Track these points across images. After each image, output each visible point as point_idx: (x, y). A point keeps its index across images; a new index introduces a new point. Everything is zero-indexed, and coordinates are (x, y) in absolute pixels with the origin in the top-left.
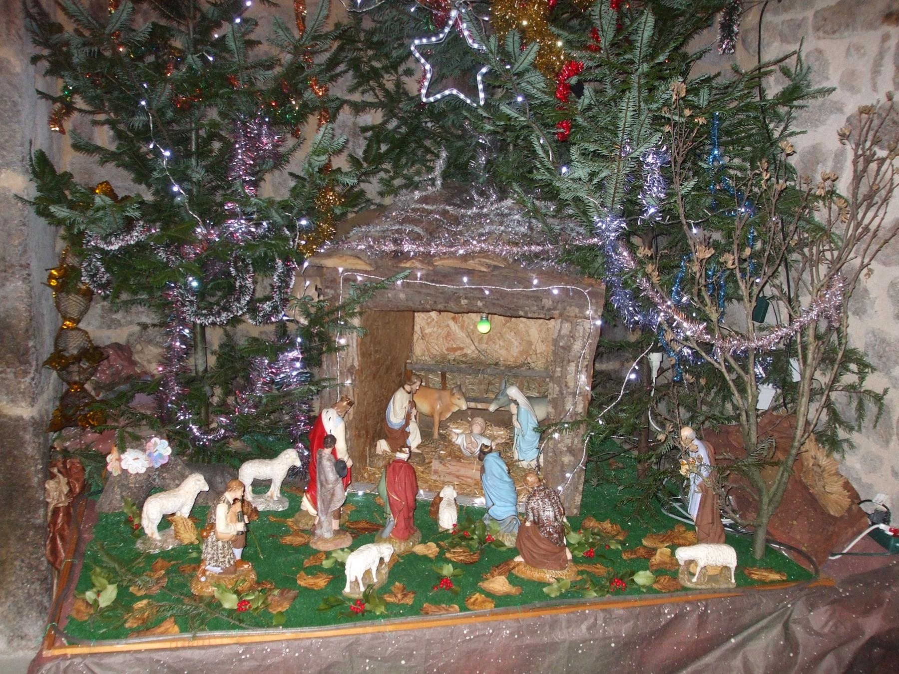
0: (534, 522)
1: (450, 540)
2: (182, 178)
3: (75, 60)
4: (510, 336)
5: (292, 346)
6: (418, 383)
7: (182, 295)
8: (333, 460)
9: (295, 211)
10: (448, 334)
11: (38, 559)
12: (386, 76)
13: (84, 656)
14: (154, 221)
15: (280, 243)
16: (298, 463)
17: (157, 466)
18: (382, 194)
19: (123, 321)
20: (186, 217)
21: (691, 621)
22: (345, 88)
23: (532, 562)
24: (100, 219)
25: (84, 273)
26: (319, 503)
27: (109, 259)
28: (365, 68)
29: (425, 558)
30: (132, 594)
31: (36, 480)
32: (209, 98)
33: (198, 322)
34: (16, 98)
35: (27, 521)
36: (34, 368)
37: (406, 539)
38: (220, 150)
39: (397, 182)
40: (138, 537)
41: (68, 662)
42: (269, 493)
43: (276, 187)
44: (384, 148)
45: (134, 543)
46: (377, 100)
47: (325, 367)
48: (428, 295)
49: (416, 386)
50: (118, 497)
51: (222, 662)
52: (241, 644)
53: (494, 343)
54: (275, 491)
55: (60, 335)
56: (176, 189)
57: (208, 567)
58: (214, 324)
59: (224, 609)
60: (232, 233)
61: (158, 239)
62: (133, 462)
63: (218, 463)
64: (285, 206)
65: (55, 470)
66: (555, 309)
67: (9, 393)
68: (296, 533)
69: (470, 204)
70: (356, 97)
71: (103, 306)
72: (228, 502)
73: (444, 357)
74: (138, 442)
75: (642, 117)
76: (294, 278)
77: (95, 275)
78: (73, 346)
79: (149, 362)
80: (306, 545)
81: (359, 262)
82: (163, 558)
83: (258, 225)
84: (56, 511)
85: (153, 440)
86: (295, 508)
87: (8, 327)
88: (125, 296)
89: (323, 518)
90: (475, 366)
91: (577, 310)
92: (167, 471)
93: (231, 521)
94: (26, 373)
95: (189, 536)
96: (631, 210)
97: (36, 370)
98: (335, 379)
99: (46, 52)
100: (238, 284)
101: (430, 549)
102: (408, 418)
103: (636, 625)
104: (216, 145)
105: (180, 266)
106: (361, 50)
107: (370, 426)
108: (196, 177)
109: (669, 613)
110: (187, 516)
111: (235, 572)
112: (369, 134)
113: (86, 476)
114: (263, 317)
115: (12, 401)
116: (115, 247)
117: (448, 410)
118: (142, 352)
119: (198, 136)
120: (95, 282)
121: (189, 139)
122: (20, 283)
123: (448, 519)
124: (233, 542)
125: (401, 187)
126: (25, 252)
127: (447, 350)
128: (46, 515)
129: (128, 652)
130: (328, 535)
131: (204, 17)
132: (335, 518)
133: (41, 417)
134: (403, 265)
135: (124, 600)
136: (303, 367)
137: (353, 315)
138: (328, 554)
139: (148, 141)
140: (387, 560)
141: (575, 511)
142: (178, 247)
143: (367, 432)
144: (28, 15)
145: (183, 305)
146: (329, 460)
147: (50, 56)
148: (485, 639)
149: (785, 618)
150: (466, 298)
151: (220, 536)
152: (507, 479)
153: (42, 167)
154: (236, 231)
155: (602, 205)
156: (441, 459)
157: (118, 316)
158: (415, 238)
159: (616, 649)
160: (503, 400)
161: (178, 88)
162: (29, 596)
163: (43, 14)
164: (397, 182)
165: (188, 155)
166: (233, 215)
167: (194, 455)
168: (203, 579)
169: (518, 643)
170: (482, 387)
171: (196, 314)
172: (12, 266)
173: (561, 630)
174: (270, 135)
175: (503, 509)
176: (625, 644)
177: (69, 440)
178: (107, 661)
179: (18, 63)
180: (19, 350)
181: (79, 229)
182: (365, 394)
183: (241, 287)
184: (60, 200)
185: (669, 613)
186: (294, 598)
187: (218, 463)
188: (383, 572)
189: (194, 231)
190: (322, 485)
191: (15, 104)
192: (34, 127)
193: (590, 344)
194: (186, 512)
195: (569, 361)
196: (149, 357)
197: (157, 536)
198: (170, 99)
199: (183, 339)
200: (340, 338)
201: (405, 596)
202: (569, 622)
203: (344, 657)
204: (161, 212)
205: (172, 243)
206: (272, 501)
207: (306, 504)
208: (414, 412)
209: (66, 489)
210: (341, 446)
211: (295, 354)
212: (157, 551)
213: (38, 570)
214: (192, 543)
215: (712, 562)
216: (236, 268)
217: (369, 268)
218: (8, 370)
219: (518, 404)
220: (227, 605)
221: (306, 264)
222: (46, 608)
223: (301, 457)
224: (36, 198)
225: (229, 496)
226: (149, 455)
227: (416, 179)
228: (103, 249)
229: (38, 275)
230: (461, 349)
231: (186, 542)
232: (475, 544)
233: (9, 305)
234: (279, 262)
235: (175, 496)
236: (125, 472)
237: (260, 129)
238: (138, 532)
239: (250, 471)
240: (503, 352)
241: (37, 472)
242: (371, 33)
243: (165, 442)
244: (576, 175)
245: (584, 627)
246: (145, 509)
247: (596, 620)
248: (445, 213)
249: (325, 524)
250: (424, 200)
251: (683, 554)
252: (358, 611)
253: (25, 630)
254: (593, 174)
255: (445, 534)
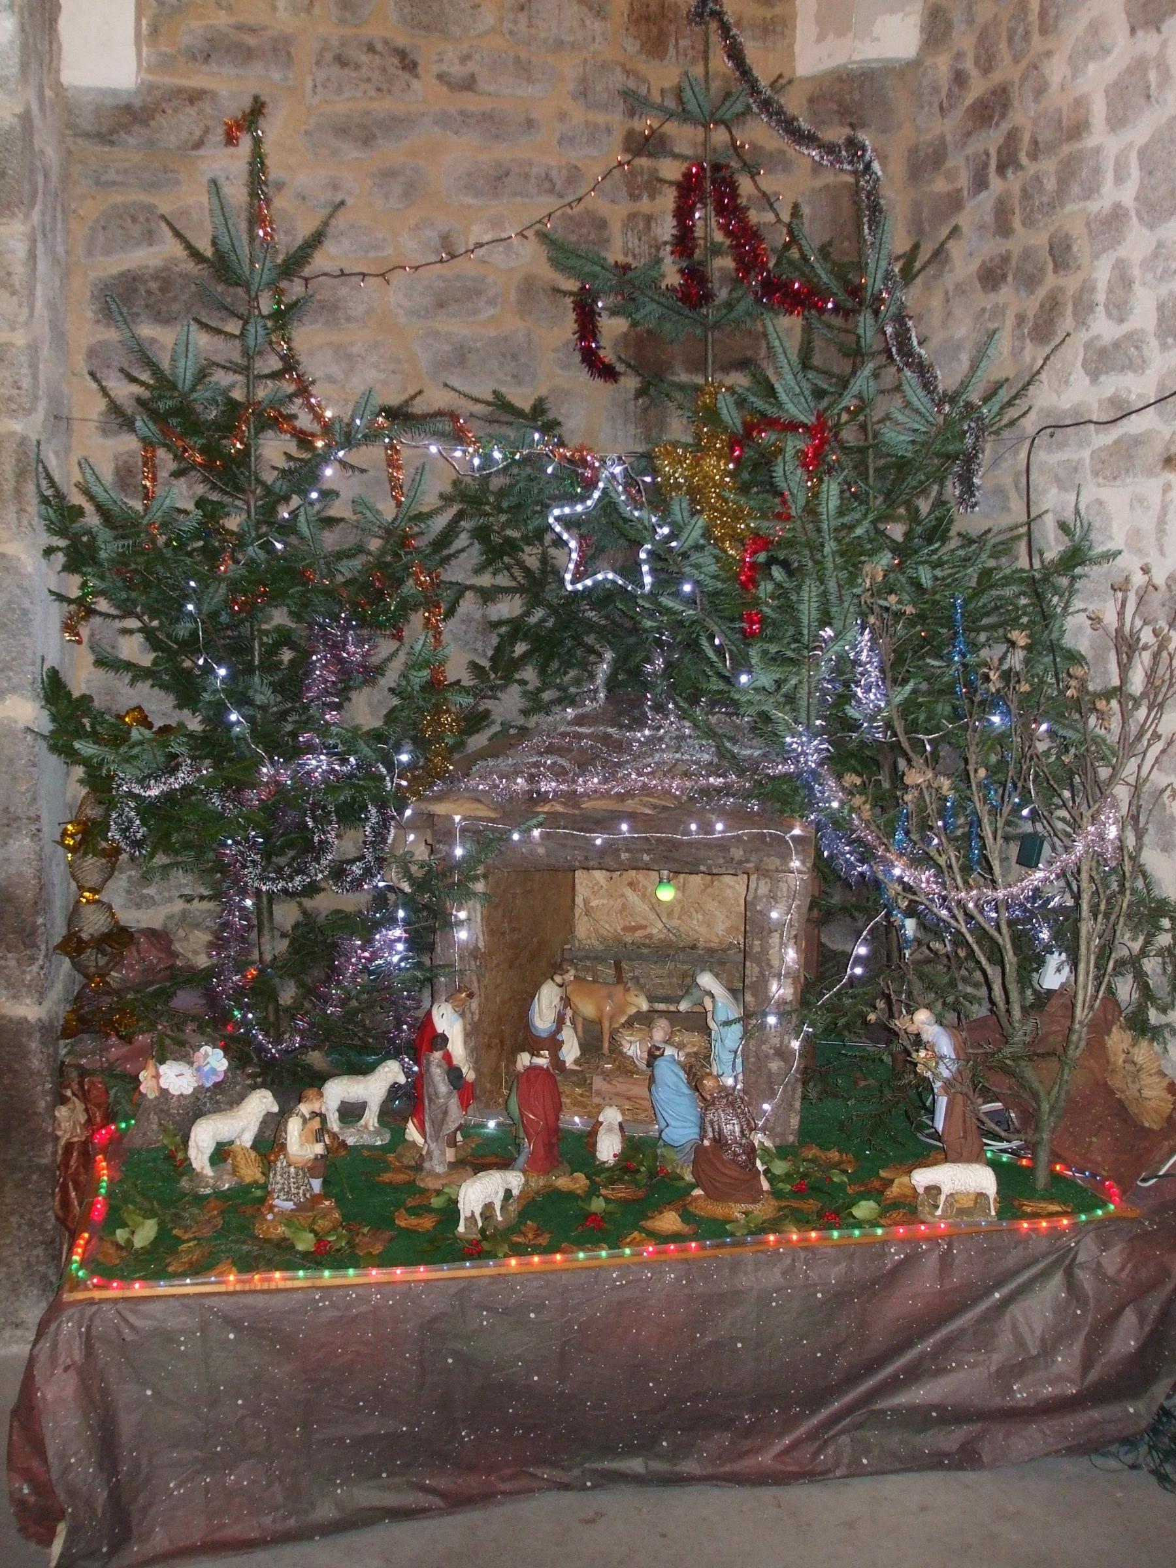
0: (714, 1139)
1: (607, 1174)
2: (242, 700)
3: (103, 555)
4: (712, 906)
5: (392, 921)
6: (572, 972)
7: (242, 853)
8: (446, 1067)
9: (392, 742)
10: (624, 907)
11: (43, 1213)
12: (527, 549)
13: (115, 1301)
14: (201, 758)
15: (371, 784)
16: (402, 1080)
17: (208, 1085)
18: (525, 713)
19: (157, 897)
20: (247, 752)
21: (931, 1263)
22: (469, 567)
23: (714, 1194)
24: (136, 757)
25: (113, 827)
26: (427, 1125)
27: (148, 809)
28: (496, 539)
29: (571, 1195)
30: (177, 1238)
31: (43, 1104)
32: (277, 598)
33: (264, 888)
34: (27, 604)
35: (30, 1161)
36: (43, 953)
37: (546, 1172)
38: (291, 661)
39: (547, 696)
40: (182, 1175)
41: (94, 1308)
42: (362, 1122)
43: (366, 709)
44: (520, 648)
45: (178, 1181)
46: (514, 584)
47: (439, 950)
48: (575, 848)
49: (570, 976)
50: (155, 1127)
51: (293, 1311)
52: (318, 1288)
53: (691, 917)
54: (371, 1118)
55: (74, 915)
56: (233, 717)
57: (276, 1202)
58: (285, 891)
59: (298, 1252)
60: (308, 773)
61: (210, 782)
62: (175, 1079)
63: (293, 1082)
64: (377, 736)
65: (69, 1093)
66: (748, 861)
67: (10, 985)
68: (399, 1170)
69: (640, 723)
70: (485, 580)
71: (130, 877)
72: (303, 1116)
73: (619, 940)
74: (182, 1051)
75: (846, 605)
76: (393, 831)
77: (128, 829)
78: (94, 923)
79: (196, 953)
80: (411, 1183)
81: (480, 806)
82: (217, 1198)
83: (344, 761)
84: (69, 1147)
85: (203, 1050)
86: (399, 1135)
87: (10, 899)
88: (161, 859)
89: (433, 1146)
90: (663, 951)
91: (778, 861)
92: (223, 1092)
93: (307, 1141)
94: (32, 959)
95: (251, 1172)
96: (840, 725)
97: (46, 956)
98: (452, 965)
99: (62, 543)
100: (316, 839)
101: (576, 1182)
102: (560, 1021)
103: (850, 1269)
104: (287, 655)
105: (239, 816)
106: (489, 515)
107: (504, 1031)
108: (260, 699)
109: (896, 1253)
110: (248, 1145)
111: (312, 1209)
112: (503, 630)
113: (111, 1100)
114: (352, 882)
115: (14, 997)
116: (154, 792)
117: (623, 1012)
118: (186, 938)
119: (262, 644)
120: (127, 838)
121: (251, 650)
122: (27, 841)
123: (608, 1148)
124: (311, 1169)
125: (552, 702)
126: (34, 800)
127: (624, 929)
128: (55, 1153)
129: (173, 1296)
130: (440, 1169)
131: (268, 490)
132: (449, 1146)
133: (51, 1021)
134: (539, 809)
135: (165, 1244)
136: (407, 950)
137: (476, 878)
138: (438, 1193)
139: (197, 652)
140: (516, 1192)
141: (791, 1138)
142: (238, 791)
143: (502, 1042)
144: (45, 500)
145: (244, 867)
146: (439, 1066)
147: (68, 547)
148: (643, 1285)
149: (1067, 1262)
150: (627, 851)
151: (292, 1159)
152: (686, 1091)
153: (54, 689)
154: (315, 770)
155: (796, 722)
156: (606, 1075)
157: (151, 891)
158: (559, 773)
159: (823, 1302)
160: (696, 994)
161: (234, 586)
162: (29, 1265)
163: (60, 496)
164: (547, 696)
165: (249, 670)
166: (310, 749)
167: (254, 1066)
168: (270, 1217)
169: (686, 1291)
170: (675, 980)
171: (263, 878)
172: (18, 818)
173: (746, 1273)
174: (359, 643)
175: (682, 1132)
176: (837, 1295)
177: (85, 1056)
178: (143, 1308)
179: (30, 561)
180: (24, 929)
181: (109, 770)
182: (497, 987)
183: (321, 842)
184: (80, 733)
185: (896, 1253)
186: (392, 1239)
187: (293, 1082)
188: (511, 1208)
189: (258, 771)
190: (430, 1100)
191: (25, 612)
192: (47, 640)
193: (798, 907)
194: (247, 1140)
195: (771, 931)
196: (195, 947)
197: (209, 1171)
198: (225, 601)
199: (244, 913)
200: (458, 910)
201: (537, 1235)
202: (756, 1264)
203: (453, 1307)
204: (213, 744)
205: (229, 786)
206: (369, 1132)
207: (412, 1133)
208: (569, 1013)
209: (83, 1118)
210: (457, 1048)
211: (398, 932)
212: (208, 1191)
213: (43, 1230)
214: (256, 1182)
215: (959, 1187)
216: (314, 818)
217: (493, 815)
218: (10, 955)
219: (713, 997)
220: (300, 1247)
221: (408, 813)
222: (51, 1283)
223: (408, 1073)
224: (52, 732)
225: (304, 1108)
226: (198, 1070)
227: (572, 690)
228: (139, 795)
229: (50, 831)
230: (644, 927)
231: (248, 1180)
232: (642, 1178)
233: (12, 870)
234: (373, 810)
235: (233, 1118)
236: (164, 1092)
237: (344, 635)
238: (185, 1167)
239: (338, 1091)
240: (703, 930)
241: (45, 1093)
242: (502, 493)
243: (220, 1053)
244: (758, 684)
245: (777, 1271)
246: (192, 1135)
247: (793, 1260)
248: (606, 738)
249: (436, 1154)
250: (579, 720)
251: (922, 1178)
252: (475, 1251)
253: (22, 1314)
254: (779, 683)
255: (601, 1168)
